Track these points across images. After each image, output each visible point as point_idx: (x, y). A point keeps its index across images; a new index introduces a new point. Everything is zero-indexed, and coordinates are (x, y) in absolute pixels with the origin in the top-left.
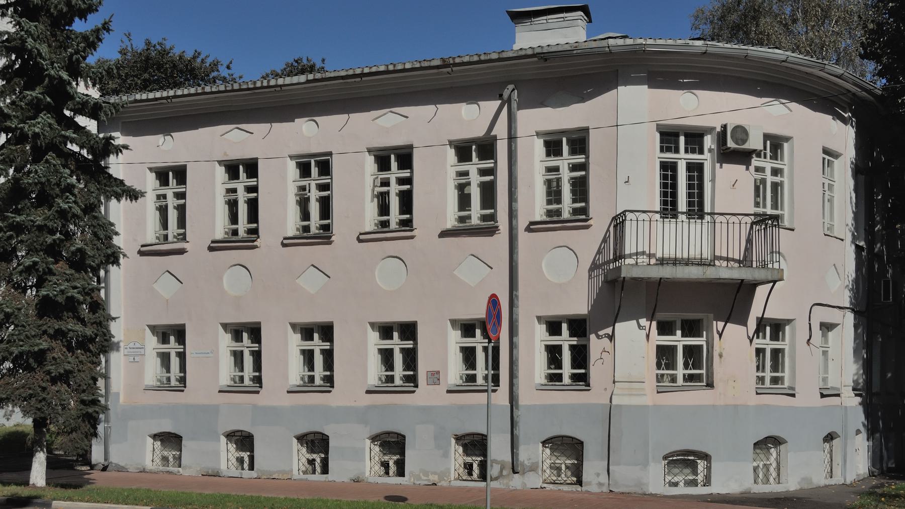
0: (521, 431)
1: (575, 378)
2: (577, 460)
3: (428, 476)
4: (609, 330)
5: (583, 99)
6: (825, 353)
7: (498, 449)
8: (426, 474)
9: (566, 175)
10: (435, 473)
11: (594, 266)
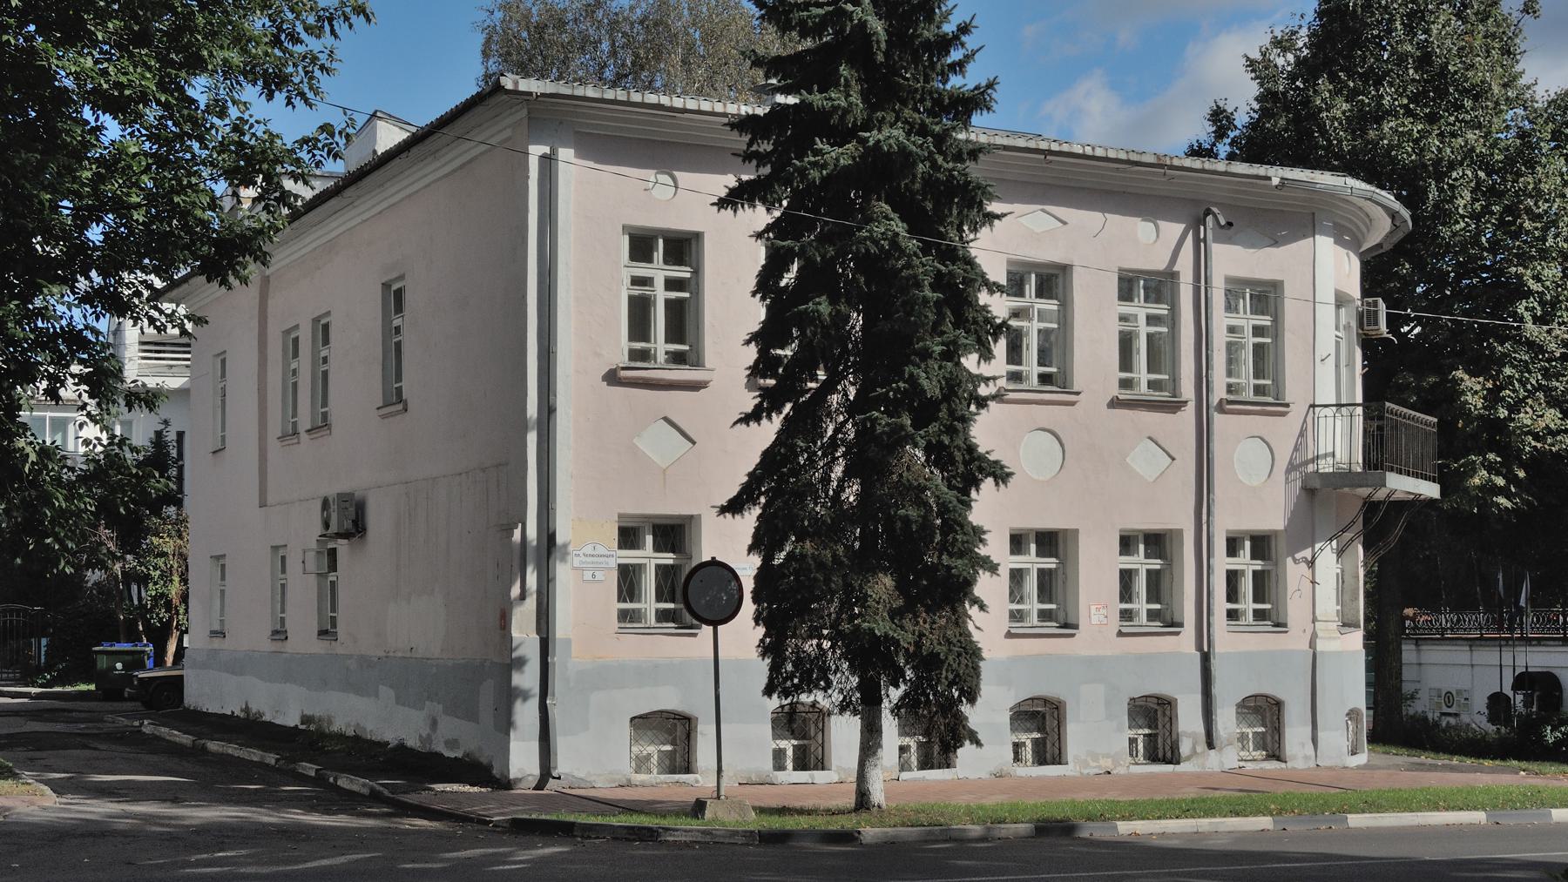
0: (1217, 690)
1: (1260, 615)
2: (1039, 731)
3: (1096, 760)
4: (1307, 553)
5: (1276, 243)
6: (1313, 582)
7: (1189, 720)
8: (1095, 757)
9: (661, 295)
10: (1108, 756)
11: (1291, 468)
